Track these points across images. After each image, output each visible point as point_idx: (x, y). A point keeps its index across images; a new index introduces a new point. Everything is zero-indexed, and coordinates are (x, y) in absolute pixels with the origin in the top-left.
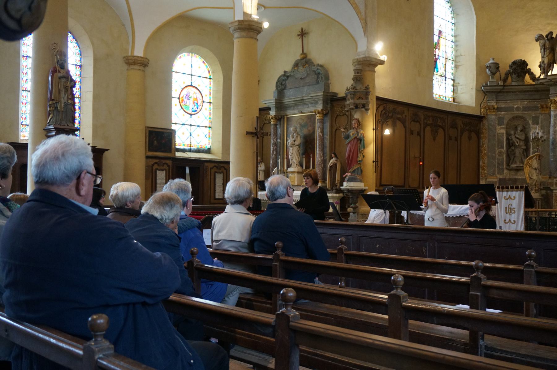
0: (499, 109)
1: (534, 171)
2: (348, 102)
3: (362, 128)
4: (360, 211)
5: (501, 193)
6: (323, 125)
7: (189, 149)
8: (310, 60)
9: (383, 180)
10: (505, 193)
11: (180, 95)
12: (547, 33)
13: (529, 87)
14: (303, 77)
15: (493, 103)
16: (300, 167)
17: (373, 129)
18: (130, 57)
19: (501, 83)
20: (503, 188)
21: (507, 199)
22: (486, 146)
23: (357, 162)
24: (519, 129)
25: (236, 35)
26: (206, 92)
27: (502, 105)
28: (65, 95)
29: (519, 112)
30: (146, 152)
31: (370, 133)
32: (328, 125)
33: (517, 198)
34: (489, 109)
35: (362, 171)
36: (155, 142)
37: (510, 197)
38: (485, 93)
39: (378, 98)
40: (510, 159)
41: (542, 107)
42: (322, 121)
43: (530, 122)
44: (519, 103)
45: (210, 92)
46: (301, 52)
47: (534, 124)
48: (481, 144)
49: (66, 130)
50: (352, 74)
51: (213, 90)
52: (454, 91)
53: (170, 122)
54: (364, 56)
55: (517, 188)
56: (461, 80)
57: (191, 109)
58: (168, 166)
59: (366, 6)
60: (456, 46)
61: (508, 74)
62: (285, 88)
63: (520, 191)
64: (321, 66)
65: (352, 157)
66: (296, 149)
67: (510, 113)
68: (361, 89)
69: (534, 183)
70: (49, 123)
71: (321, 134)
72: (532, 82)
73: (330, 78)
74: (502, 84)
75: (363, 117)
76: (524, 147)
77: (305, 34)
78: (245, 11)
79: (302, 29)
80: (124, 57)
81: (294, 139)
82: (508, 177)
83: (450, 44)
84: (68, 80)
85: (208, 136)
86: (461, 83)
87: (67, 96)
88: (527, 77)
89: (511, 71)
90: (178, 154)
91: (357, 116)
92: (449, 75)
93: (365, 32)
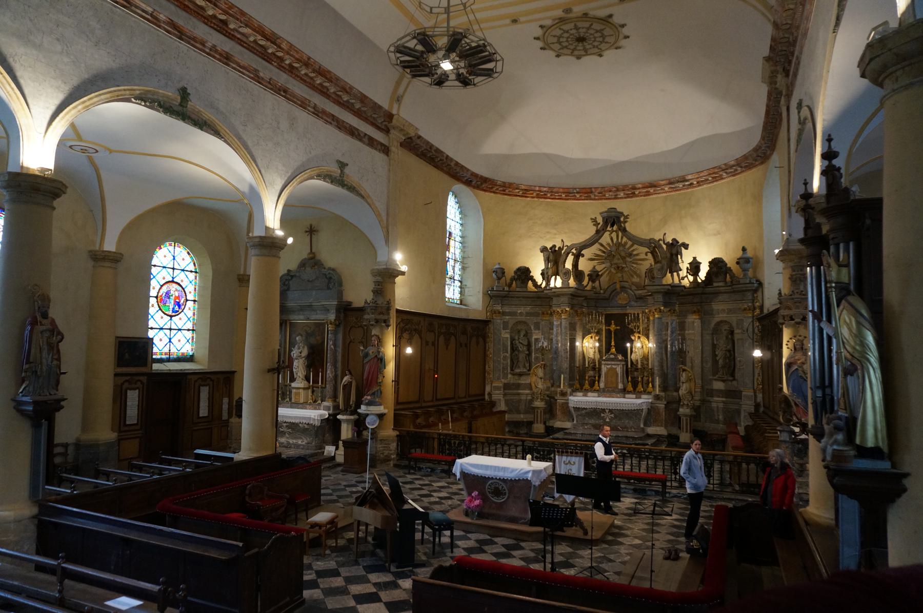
0: (504, 314)
1: (539, 380)
2: (366, 317)
3: (382, 346)
4: (379, 436)
5: (560, 457)
6: (335, 337)
7: (167, 358)
8: (319, 261)
9: (399, 398)
10: (564, 458)
11: (158, 293)
12: (551, 246)
13: (532, 293)
14: (311, 280)
15: (498, 307)
16: (306, 382)
17: (393, 346)
18: (98, 251)
19: (506, 289)
20: (562, 452)
21: (567, 464)
22: (491, 350)
23: (377, 383)
24: (522, 334)
25: (252, 252)
26: (190, 289)
27: (507, 309)
28: (49, 355)
29: (523, 317)
30: (115, 369)
31: (390, 350)
32: (340, 336)
33: (577, 463)
34: (495, 313)
35: (381, 392)
36: (127, 354)
37: (569, 462)
38: (491, 297)
39: (398, 311)
40: (514, 363)
41: (543, 314)
42: (335, 333)
43: (532, 327)
44: (522, 309)
45: (195, 289)
46: (310, 251)
47: (535, 330)
48: (487, 348)
49: (49, 402)
50: (371, 286)
51: (199, 286)
52: (461, 293)
53: (147, 328)
54: (385, 267)
55: (577, 453)
56: (468, 283)
57: (171, 309)
58: (142, 383)
59: (388, 214)
60: (464, 247)
61: (513, 279)
62: (288, 289)
63: (580, 456)
64: (333, 270)
65: (372, 379)
66: (301, 361)
67: (514, 317)
68: (382, 303)
69: (539, 392)
70: (21, 392)
71: (332, 346)
72: (534, 289)
73: (344, 283)
74: (508, 289)
75: (382, 333)
76: (527, 352)
77: (315, 231)
78: (267, 225)
79: (311, 226)
80: (90, 251)
81: (300, 351)
82: (512, 382)
83: (458, 245)
84: (53, 334)
85: (190, 341)
86: (468, 285)
87: (52, 356)
88: (530, 283)
89: (516, 277)
90: (156, 366)
91: (375, 331)
92: (457, 277)
93: (387, 241)
